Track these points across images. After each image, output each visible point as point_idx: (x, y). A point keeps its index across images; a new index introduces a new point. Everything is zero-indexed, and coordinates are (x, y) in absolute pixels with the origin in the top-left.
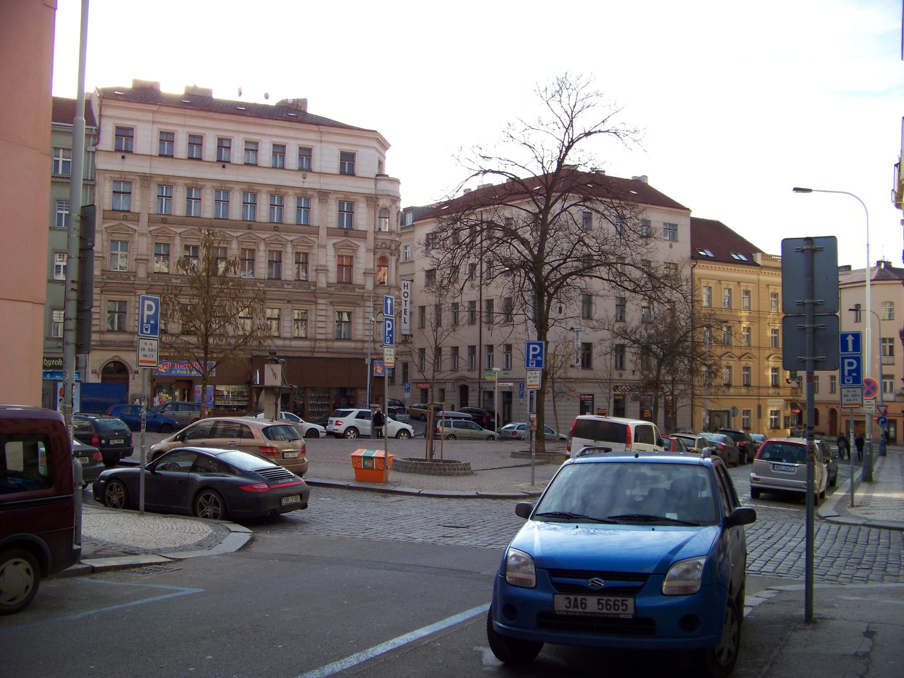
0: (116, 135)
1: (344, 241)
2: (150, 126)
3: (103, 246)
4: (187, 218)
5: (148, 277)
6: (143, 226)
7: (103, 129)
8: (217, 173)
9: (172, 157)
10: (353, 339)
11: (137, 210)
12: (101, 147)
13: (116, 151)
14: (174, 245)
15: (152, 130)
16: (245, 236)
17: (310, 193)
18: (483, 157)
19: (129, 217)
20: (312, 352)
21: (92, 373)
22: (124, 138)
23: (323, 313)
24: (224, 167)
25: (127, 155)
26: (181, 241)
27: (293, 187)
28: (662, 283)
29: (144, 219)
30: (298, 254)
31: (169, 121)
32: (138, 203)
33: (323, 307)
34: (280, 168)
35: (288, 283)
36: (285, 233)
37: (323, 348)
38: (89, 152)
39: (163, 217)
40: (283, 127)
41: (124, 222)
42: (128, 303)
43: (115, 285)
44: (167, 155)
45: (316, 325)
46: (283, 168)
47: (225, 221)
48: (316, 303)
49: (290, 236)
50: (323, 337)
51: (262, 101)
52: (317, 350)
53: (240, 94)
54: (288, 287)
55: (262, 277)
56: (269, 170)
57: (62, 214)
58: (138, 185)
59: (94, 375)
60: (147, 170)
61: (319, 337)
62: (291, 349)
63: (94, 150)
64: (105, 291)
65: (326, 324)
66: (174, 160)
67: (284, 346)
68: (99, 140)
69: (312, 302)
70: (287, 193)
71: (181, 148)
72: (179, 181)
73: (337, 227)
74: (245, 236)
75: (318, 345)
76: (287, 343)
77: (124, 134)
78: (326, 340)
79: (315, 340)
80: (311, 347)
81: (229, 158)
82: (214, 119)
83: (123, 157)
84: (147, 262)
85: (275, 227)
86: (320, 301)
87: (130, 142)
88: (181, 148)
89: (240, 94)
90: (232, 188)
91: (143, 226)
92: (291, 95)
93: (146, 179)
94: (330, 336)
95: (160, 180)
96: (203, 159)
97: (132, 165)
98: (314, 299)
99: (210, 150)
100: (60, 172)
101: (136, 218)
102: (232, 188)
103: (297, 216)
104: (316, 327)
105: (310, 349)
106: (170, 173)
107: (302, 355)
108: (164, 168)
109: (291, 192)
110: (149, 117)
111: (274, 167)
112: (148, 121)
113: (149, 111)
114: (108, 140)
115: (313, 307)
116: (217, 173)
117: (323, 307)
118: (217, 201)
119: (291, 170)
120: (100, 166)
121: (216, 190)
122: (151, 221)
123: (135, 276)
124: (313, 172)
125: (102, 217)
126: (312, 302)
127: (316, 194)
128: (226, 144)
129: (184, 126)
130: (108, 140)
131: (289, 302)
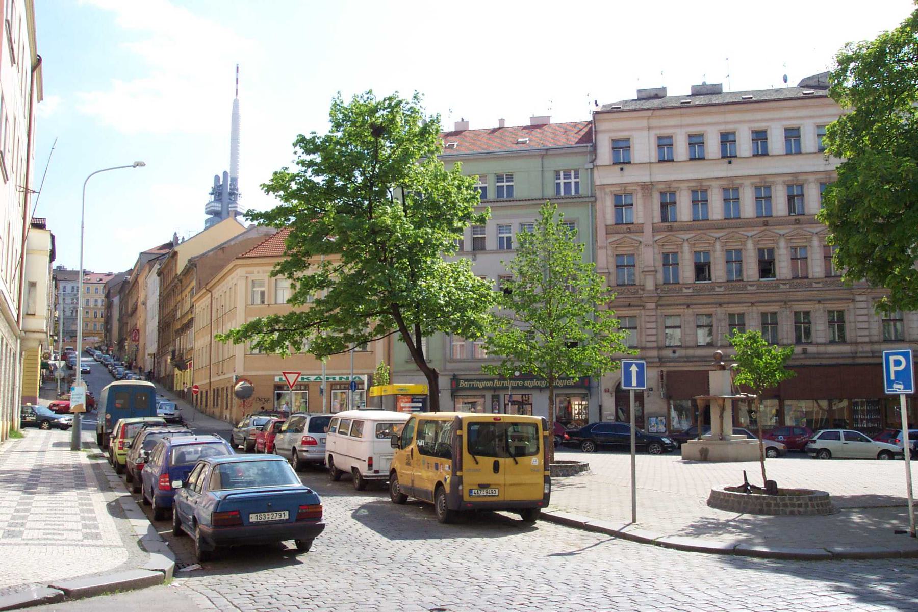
0: (613, 148)
1: (795, 229)
2: (645, 133)
3: (654, 260)
4: (694, 223)
5: (657, 289)
6: (647, 236)
7: (599, 145)
8: (723, 171)
9: (672, 161)
10: (907, 338)
11: (641, 221)
12: (599, 162)
13: (723, 157)
14: (682, 253)
15: (649, 137)
16: (761, 235)
17: (630, 188)
18: (134, 167)
19: (632, 230)
20: (854, 358)
21: (605, 391)
22: (792, 139)
23: (864, 312)
24: (730, 162)
25: (625, 167)
26: (690, 248)
27: (813, 173)
28: (891, 243)
29: (648, 229)
30: (729, 252)
31: (666, 124)
32: (641, 214)
33: (864, 305)
34: (795, 154)
35: (751, 283)
36: (809, 225)
37: (867, 352)
38: (587, 169)
39: (765, 219)
40: (794, 107)
41: (628, 235)
42: (778, 314)
43: (623, 300)
44: (666, 159)
45: (856, 326)
46: (799, 152)
47: (736, 221)
48: (853, 300)
49: (748, 231)
50: (867, 339)
51: (781, 85)
52: (859, 355)
53: (786, 81)
54: (785, 287)
55: (817, 275)
56: (609, 168)
57: (503, 237)
58: (640, 195)
59: (607, 394)
60: (646, 179)
61: (860, 340)
62: (827, 356)
63: (592, 167)
64: (661, 306)
65: (869, 325)
66: (675, 164)
67: (818, 354)
68: (596, 156)
69: (850, 299)
70: (806, 180)
71: (681, 150)
72: (713, 183)
73: (755, 216)
74: (761, 235)
75: (860, 349)
76: (822, 349)
77: (621, 147)
78: (871, 343)
79: (857, 343)
80: (852, 353)
81: (672, 157)
82: (811, 106)
83: (622, 169)
84: (654, 273)
85: (668, 226)
86: (858, 298)
87: (733, 146)
88: (681, 150)
89: (786, 81)
90: (741, 184)
91: (647, 236)
92: (658, 85)
93: (647, 187)
94: (876, 338)
95: (662, 186)
96: (738, 156)
97: (632, 176)
98: (851, 297)
99: (713, 147)
100: (562, 193)
101: (640, 229)
102: (741, 184)
103: (757, 209)
104: (656, 328)
105: (851, 355)
106: (673, 178)
107: (841, 361)
108: (663, 174)
109: (812, 178)
110: (644, 123)
111: (789, 153)
112: (642, 129)
113: (642, 117)
114: (605, 153)
115: (851, 306)
116: (723, 171)
117: (864, 305)
118: (726, 200)
119: (778, 155)
120: (598, 182)
121: (756, 188)
122: (655, 230)
123: (643, 290)
124: (677, 162)
125: (605, 233)
126: (850, 299)
127: (638, 188)
128: (731, 138)
129: (681, 126)
130: (605, 153)
131: (819, 302)
